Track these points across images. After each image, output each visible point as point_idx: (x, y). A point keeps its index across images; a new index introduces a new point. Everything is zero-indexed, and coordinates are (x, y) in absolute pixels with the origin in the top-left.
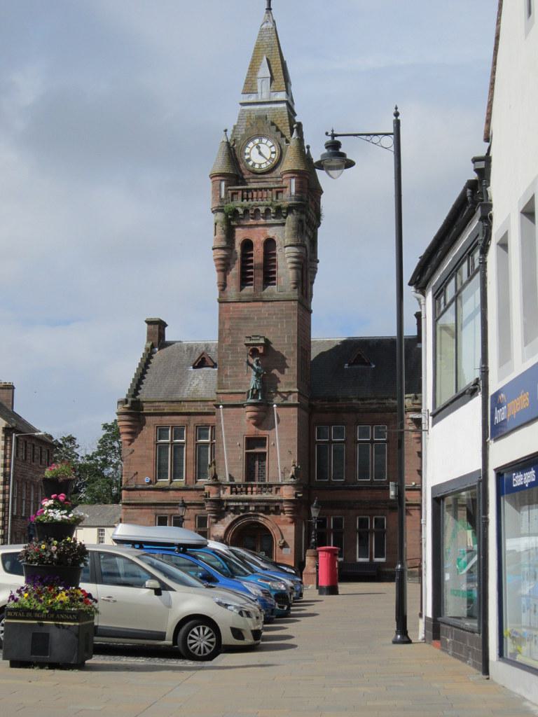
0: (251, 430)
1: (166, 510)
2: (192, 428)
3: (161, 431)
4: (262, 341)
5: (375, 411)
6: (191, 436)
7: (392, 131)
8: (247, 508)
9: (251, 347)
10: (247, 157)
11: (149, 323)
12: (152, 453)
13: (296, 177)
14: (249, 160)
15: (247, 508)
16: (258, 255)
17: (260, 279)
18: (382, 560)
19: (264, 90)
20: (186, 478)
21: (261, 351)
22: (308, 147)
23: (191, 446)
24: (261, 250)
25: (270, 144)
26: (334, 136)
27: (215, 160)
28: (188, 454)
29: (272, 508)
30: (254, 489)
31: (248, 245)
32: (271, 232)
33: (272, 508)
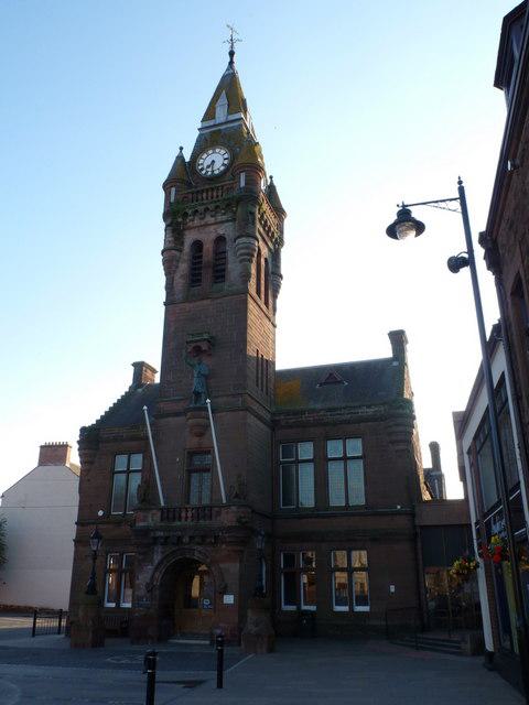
5: (348, 422)
7: (458, 196)
8: (179, 538)
9: (193, 345)
11: (135, 365)
13: (363, 592)
14: (223, 164)
15: (179, 538)
18: (366, 609)
19: (221, 114)
22: (271, 177)
25: (223, 152)
26: (404, 206)
31: (198, 245)
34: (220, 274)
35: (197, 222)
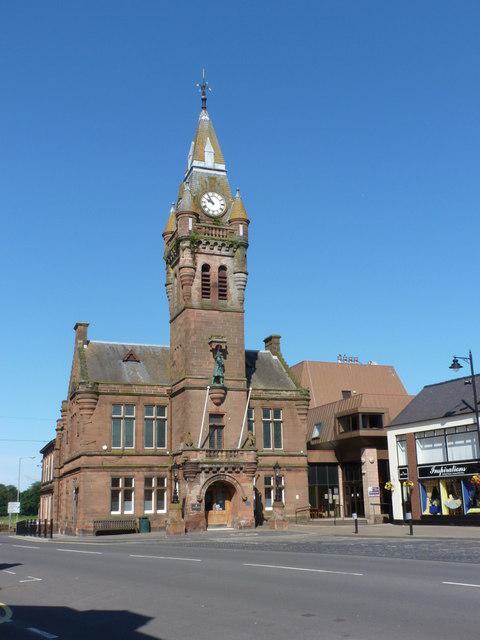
0: (214, 409)
31: (206, 268)
32: (225, 261)
35: (207, 250)
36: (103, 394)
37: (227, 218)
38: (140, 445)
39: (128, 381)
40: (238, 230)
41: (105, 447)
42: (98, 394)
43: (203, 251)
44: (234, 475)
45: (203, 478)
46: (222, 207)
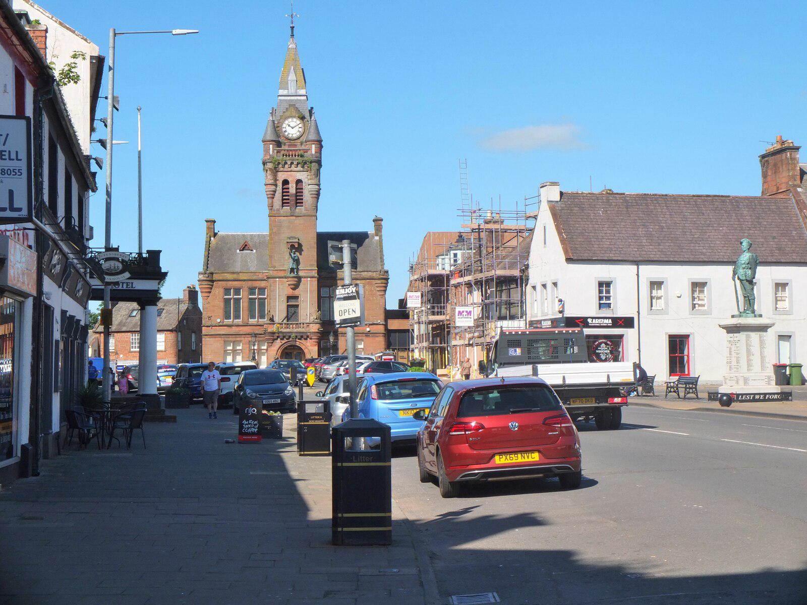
0: (290, 292)
1: (231, 339)
2: (246, 289)
3: (227, 291)
4: (297, 240)
6: (246, 293)
10: (284, 130)
12: (222, 304)
14: (285, 131)
16: (292, 189)
17: (294, 202)
20: (243, 320)
21: (296, 246)
23: (246, 300)
24: (294, 185)
27: (263, 129)
28: (244, 305)
29: (304, 336)
30: (294, 326)
31: (286, 182)
33: (304, 336)
34: (298, 200)
36: (215, 281)
37: (303, 139)
38: (246, 317)
39: (238, 269)
40: (310, 149)
41: (219, 320)
42: (213, 281)
43: (282, 169)
44: (303, 341)
45: (278, 343)
46: (286, 133)
